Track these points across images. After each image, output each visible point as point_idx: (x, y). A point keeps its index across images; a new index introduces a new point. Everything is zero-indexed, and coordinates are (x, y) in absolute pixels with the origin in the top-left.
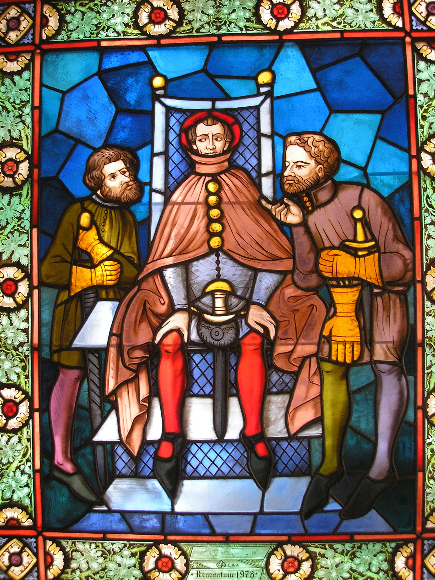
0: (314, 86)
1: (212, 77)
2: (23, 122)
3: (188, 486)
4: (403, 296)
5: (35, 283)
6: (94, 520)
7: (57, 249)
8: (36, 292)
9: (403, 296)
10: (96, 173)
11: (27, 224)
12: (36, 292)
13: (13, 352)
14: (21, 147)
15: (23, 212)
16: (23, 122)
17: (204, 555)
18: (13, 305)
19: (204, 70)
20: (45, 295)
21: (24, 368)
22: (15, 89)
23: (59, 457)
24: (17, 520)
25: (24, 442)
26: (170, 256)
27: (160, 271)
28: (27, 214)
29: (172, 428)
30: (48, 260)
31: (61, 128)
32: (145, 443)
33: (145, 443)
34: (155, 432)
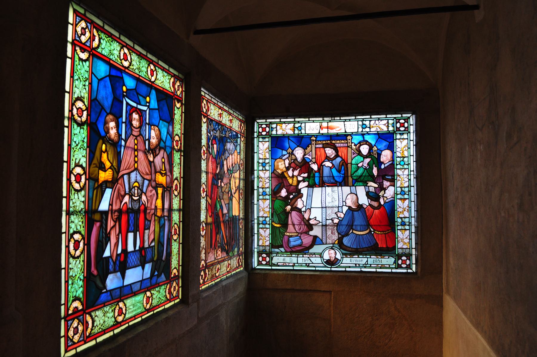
0: (125, 285)
1: (138, 94)
2: (85, 89)
3: (129, 272)
4: (169, 191)
5: (87, 177)
6: (103, 297)
7: (95, 161)
8: (87, 181)
9: (169, 191)
10: (107, 125)
11: (85, 145)
12: (87, 181)
13: (81, 78)
14: (84, 102)
15: (84, 138)
16: (85, 89)
17: (178, 90)
18: (79, 188)
19: (135, 89)
20: (91, 184)
21: (82, 222)
22: (80, 156)
23: (93, 269)
24: (81, 51)
25: (81, 262)
26: (125, 169)
27: (122, 176)
28: (85, 140)
29: (124, 248)
30: (92, 166)
31: (99, 78)
32: (117, 255)
33: (117, 255)
34: (119, 251)
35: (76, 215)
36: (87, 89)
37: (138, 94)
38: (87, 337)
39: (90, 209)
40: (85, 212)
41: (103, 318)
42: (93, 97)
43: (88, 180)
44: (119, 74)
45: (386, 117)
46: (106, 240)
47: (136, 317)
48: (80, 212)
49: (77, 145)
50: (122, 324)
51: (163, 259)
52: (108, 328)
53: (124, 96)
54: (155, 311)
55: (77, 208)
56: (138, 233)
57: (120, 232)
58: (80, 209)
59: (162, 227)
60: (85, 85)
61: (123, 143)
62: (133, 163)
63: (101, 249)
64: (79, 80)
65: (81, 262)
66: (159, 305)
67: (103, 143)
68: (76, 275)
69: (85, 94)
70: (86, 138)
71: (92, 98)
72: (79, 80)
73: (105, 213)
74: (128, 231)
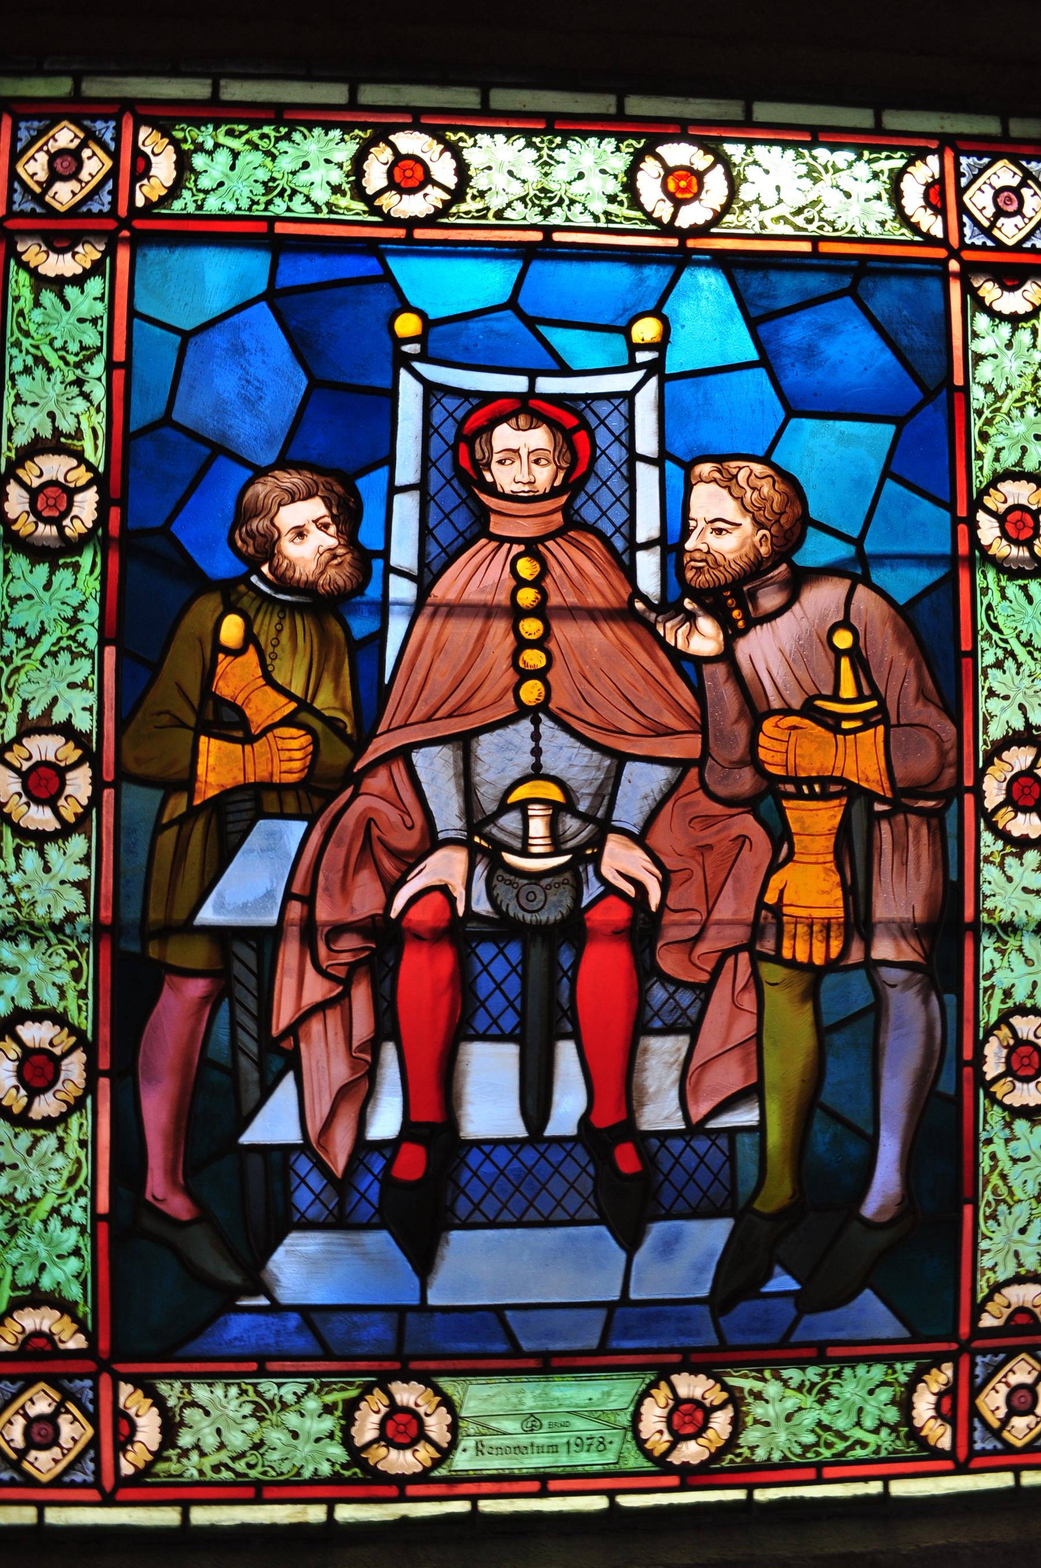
1: (531, 323)
6: (238, 1329)
7: (163, 695)
9: (935, 818)
11: (90, 636)
14: (79, 456)
19: (512, 304)
21: (76, 975)
23: (156, 1183)
25: (72, 1148)
29: (428, 1113)
32: (362, 1146)
33: (362, 1146)
34: (386, 1121)
35: (33, 940)
36: (99, 393)
37: (531, 323)
38: (122, 1482)
39: (132, 913)
40: (97, 929)
41: (251, 1425)
42: (146, 410)
43: (115, 785)
44: (369, 266)
45: (352, 105)
46: (260, 1065)
47: (553, 1485)
48: (57, 928)
49: (32, 643)
50: (411, 1490)
51: (870, 1208)
52: (287, 1483)
53: (405, 361)
54: (762, 1495)
55: (41, 910)
56: (567, 1053)
57: (387, 1025)
58: (58, 915)
59: (849, 1032)
60: (79, 382)
61: (402, 590)
62: (509, 677)
63: (218, 1099)
64: (1009, 664)
65: (72, 1148)
66: (819, 1466)
67: (230, 608)
68: (34, 1199)
69: (88, 419)
70: (93, 607)
71: (133, 428)
72: (1009, 664)
73: (264, 941)
74: (463, 1029)
